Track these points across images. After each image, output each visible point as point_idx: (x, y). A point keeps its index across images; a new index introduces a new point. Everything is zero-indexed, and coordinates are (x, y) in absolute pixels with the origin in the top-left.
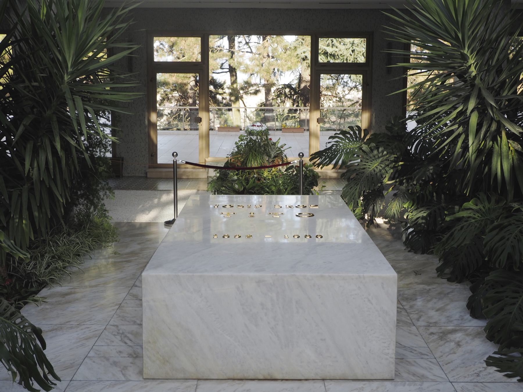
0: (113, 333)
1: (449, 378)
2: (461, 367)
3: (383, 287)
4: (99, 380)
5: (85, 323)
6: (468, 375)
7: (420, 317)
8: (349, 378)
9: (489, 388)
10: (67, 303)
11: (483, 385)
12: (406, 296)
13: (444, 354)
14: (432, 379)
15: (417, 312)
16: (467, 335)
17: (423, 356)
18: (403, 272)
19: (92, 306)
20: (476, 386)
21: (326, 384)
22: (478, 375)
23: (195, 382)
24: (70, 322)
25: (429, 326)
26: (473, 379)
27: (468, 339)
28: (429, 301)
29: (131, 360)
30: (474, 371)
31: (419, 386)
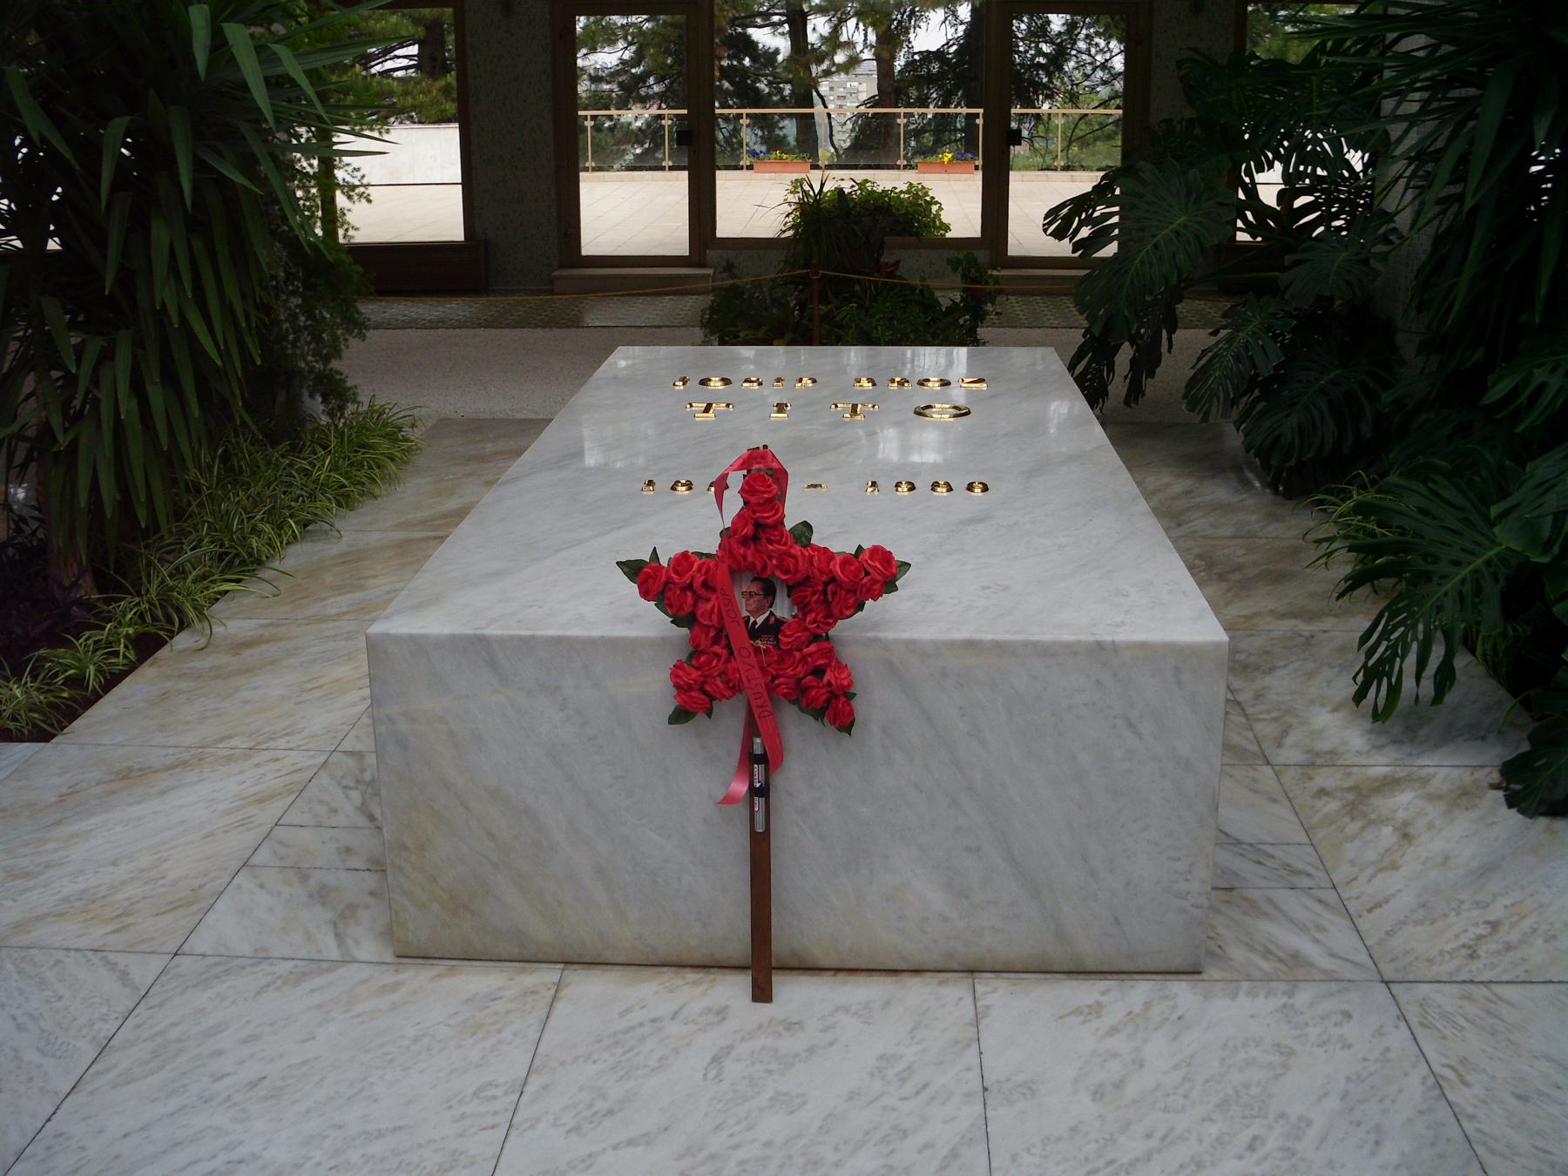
0: (345, 782)
1: (1381, 966)
2: (1418, 923)
3: (1179, 683)
4: (261, 957)
5: (272, 744)
6: (1441, 953)
7: (1285, 733)
8: (1056, 968)
9: (1510, 1004)
10: (241, 672)
11: (1488, 994)
12: (1242, 657)
13: (1362, 870)
14: (1324, 971)
15: (1274, 714)
16: (1432, 798)
17: (1295, 879)
18: (1235, 577)
19: (309, 686)
20: (1469, 998)
21: (980, 989)
22: (1473, 956)
23: (550, 974)
24: (230, 737)
25: (1312, 765)
26: (1458, 969)
27: (1433, 811)
28: (1311, 675)
29: (371, 880)
30: (1457, 936)
31: (1284, 1000)
